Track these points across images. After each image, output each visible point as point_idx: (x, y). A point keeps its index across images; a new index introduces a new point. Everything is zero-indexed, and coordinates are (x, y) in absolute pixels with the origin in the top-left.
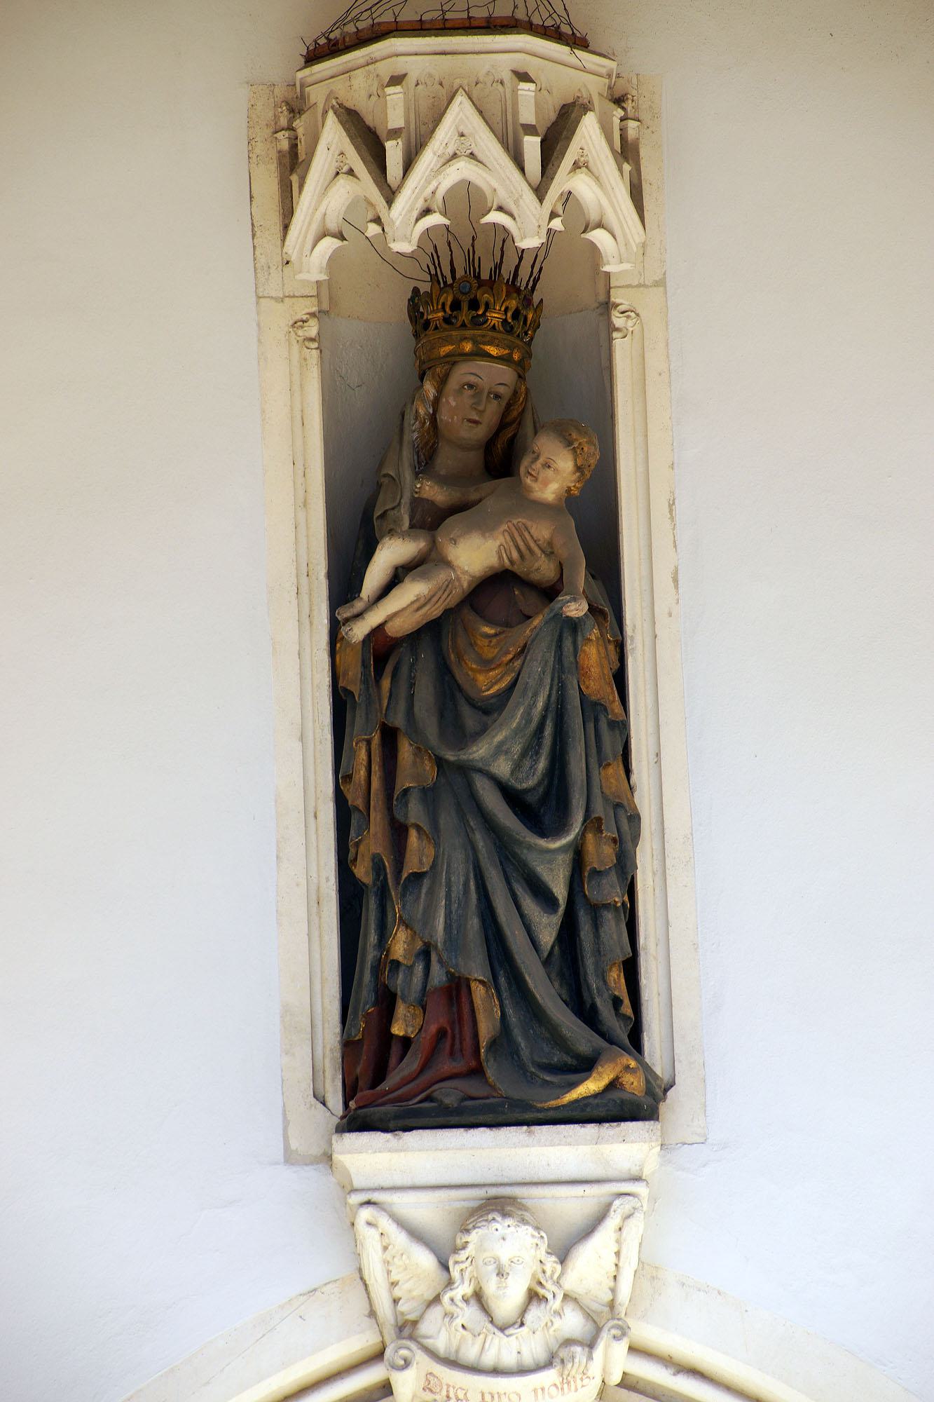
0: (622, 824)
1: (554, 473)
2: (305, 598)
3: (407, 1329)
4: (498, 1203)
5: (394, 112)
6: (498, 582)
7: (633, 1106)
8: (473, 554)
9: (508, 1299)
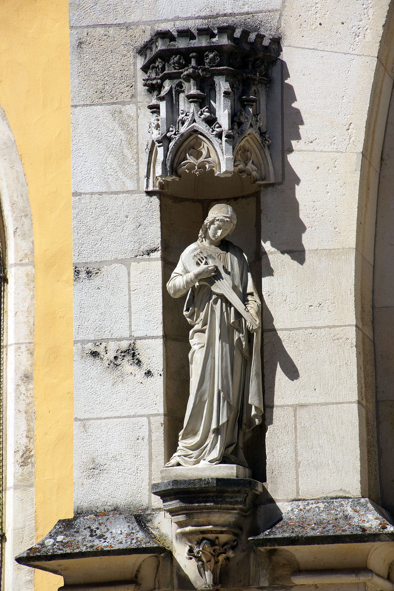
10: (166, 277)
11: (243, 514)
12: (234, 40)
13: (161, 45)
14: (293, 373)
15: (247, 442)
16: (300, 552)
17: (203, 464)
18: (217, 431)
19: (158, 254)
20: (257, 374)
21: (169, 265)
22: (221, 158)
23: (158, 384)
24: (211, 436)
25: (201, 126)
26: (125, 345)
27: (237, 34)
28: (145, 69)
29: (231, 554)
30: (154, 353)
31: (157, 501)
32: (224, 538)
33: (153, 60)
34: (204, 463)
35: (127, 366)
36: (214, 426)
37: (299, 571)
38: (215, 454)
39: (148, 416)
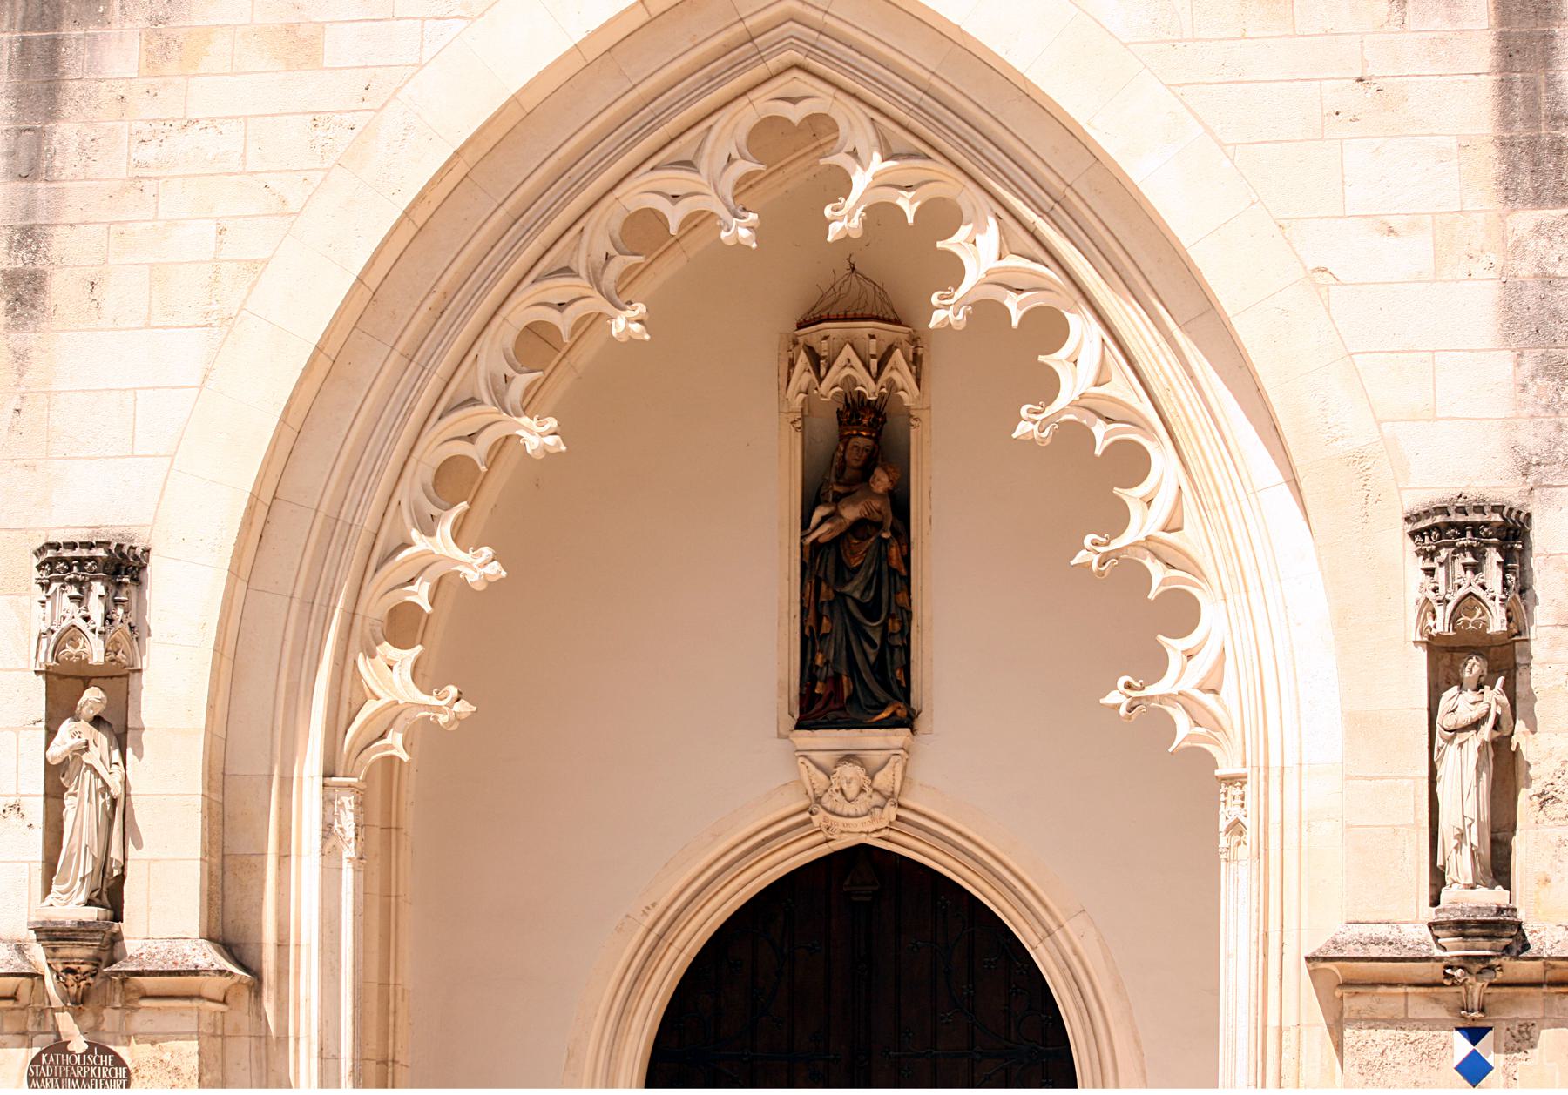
0: (906, 615)
1: (881, 481)
2: (1273, 1022)
3: (818, 799)
4: (849, 758)
5: (823, 348)
6: (859, 527)
7: (907, 721)
8: (851, 513)
9: (852, 791)
10: (47, 748)
11: (101, 949)
12: (109, 551)
13: (50, 553)
14: (139, 845)
15: (109, 893)
16: (147, 983)
17: (71, 906)
18: (83, 879)
19: (43, 724)
20: (344, 610)
21: (51, 733)
22: (95, 652)
23: (37, 837)
24: (78, 883)
25: (81, 624)
26: (12, 801)
27: (113, 547)
28: (39, 568)
29: (91, 980)
30: (35, 808)
31: (33, 935)
32: (84, 968)
33: (44, 563)
34: (71, 908)
35: (13, 815)
36: (81, 875)
37: (145, 997)
38: (82, 897)
39: (29, 862)
